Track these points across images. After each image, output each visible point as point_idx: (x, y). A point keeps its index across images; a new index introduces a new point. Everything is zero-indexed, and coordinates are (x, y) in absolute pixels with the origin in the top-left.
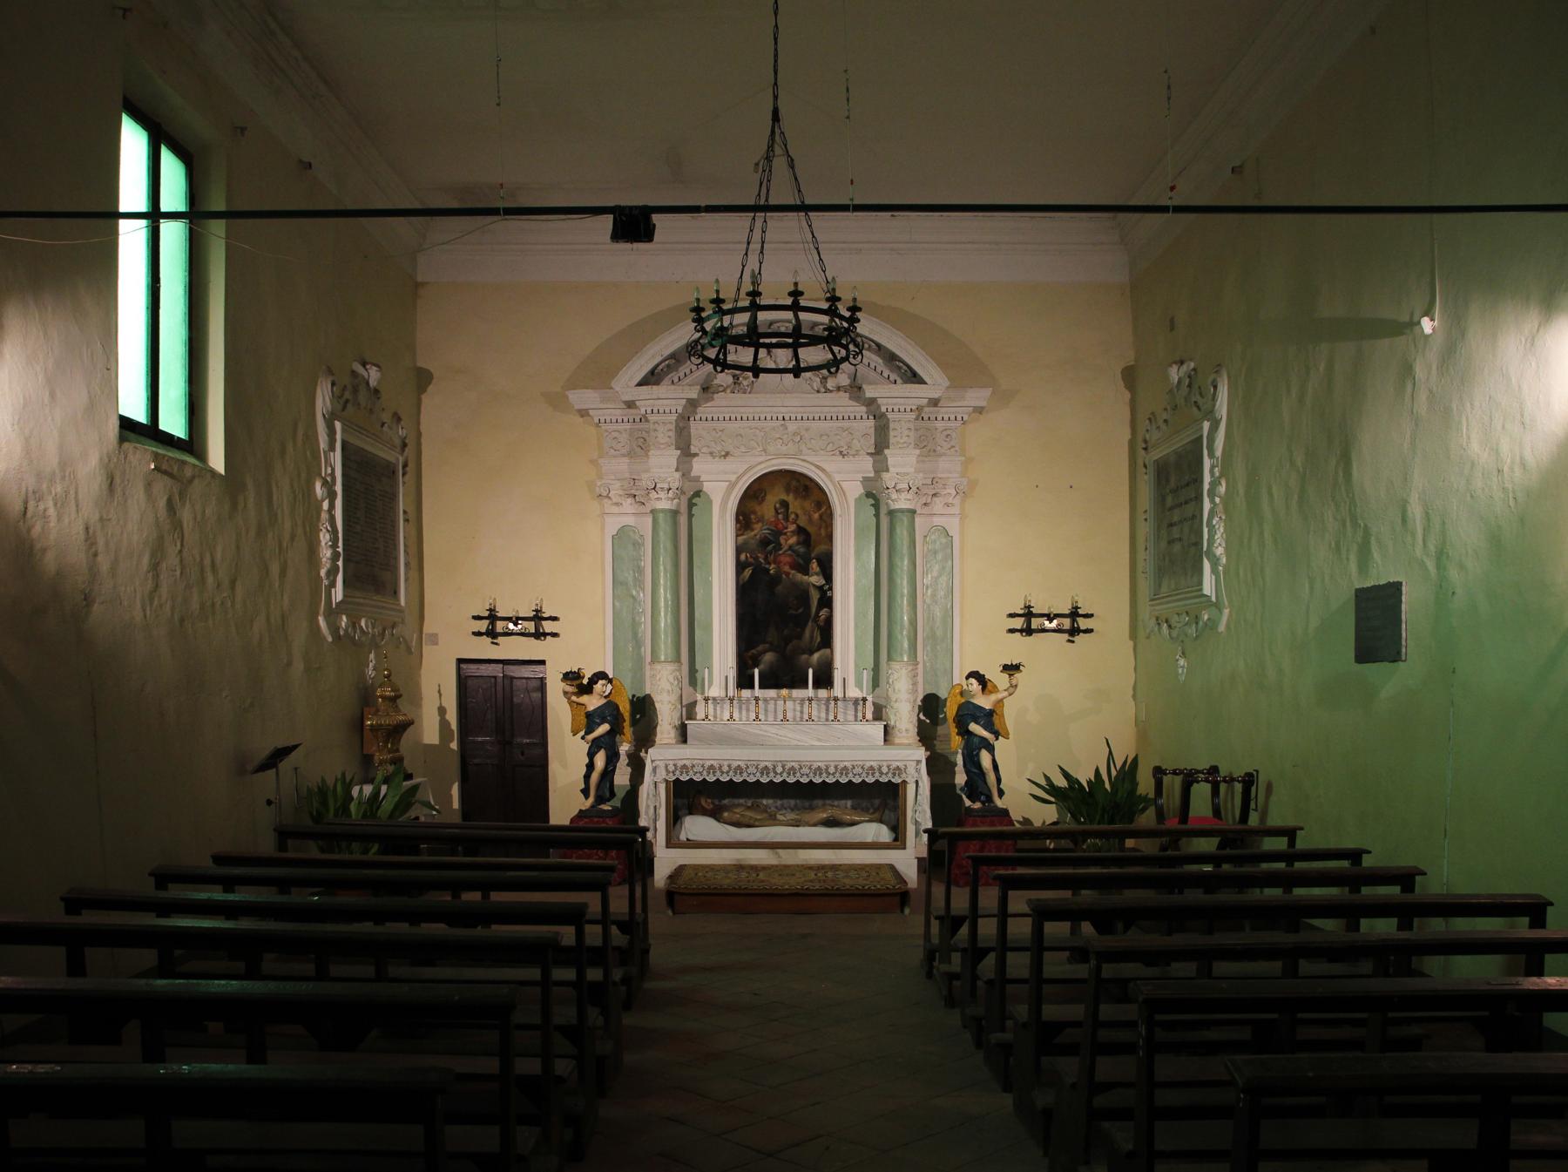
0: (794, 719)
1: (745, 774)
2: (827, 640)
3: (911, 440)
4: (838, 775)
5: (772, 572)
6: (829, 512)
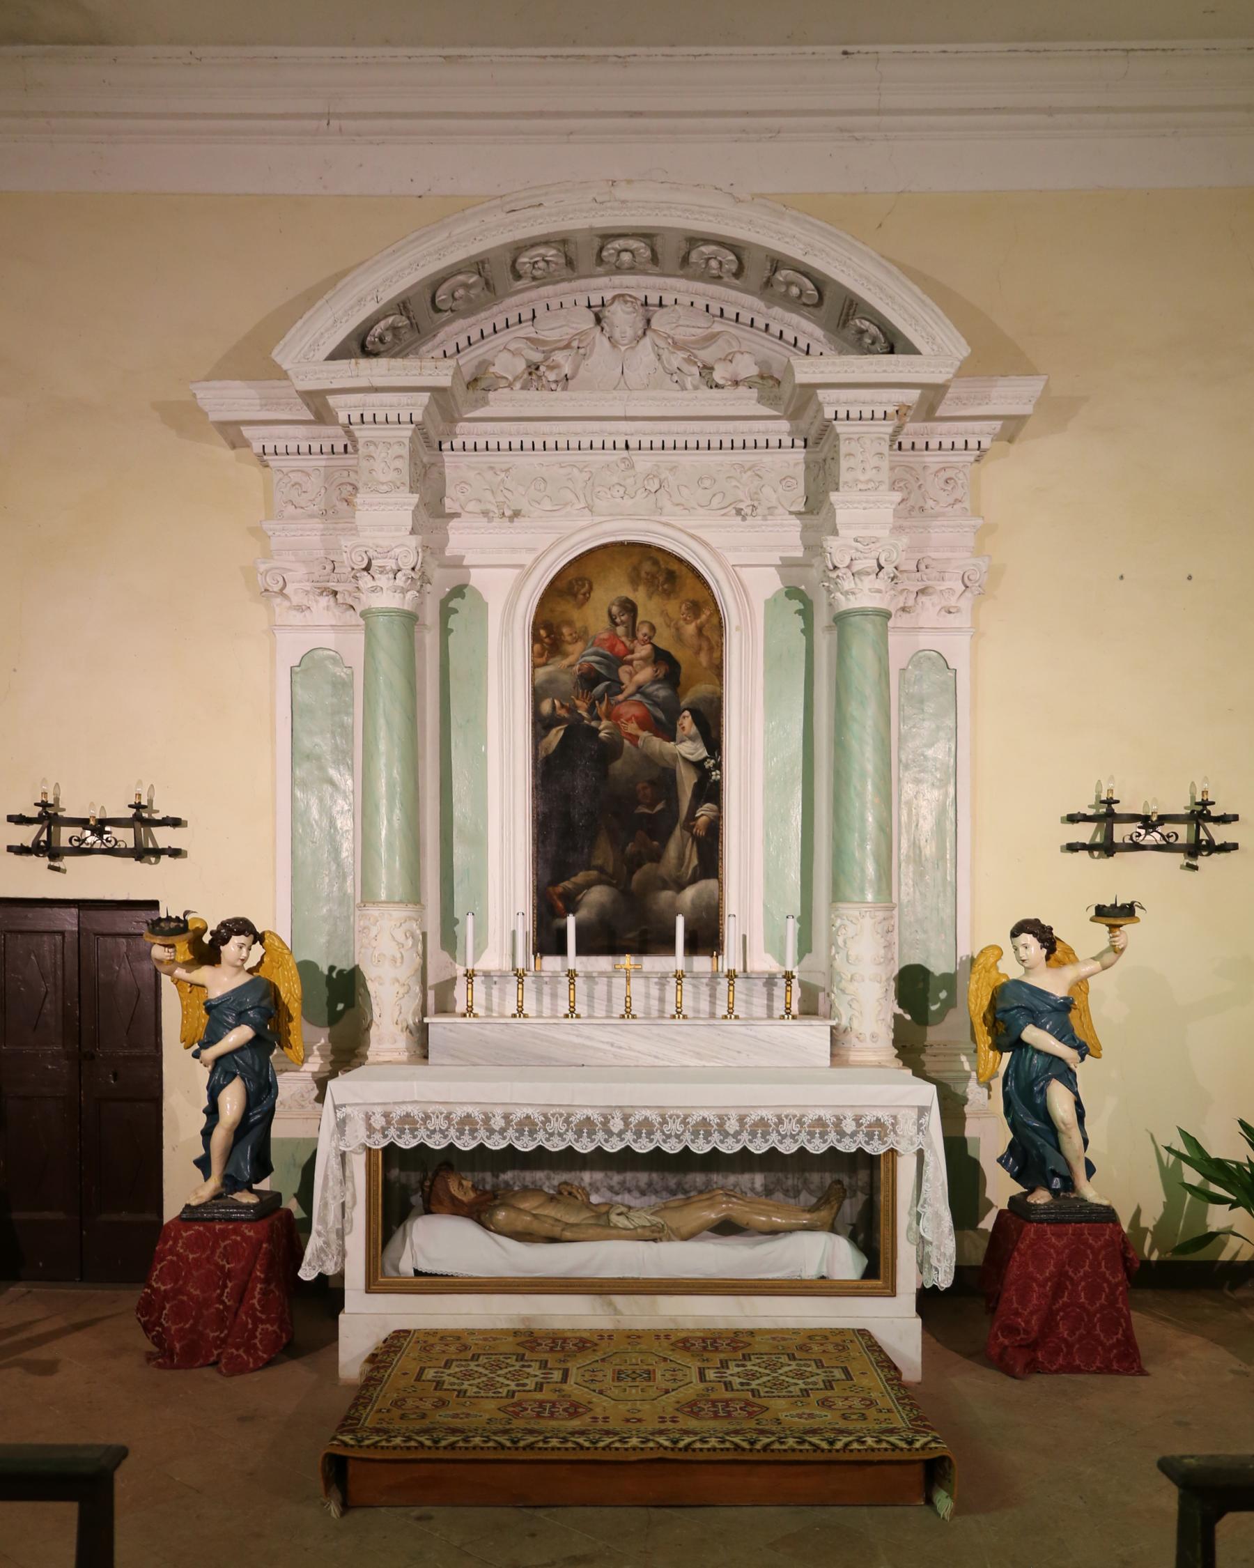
0: (648, 1016)
1: (541, 1135)
2: (710, 864)
3: (885, 475)
4: (745, 1136)
5: (602, 734)
6: (715, 620)
